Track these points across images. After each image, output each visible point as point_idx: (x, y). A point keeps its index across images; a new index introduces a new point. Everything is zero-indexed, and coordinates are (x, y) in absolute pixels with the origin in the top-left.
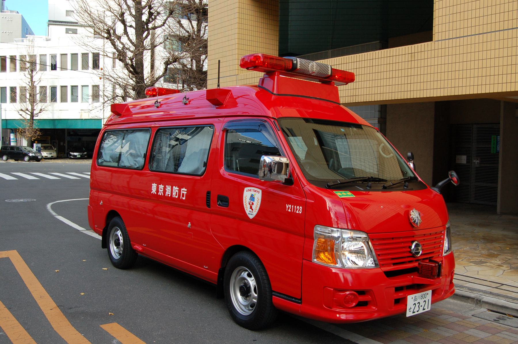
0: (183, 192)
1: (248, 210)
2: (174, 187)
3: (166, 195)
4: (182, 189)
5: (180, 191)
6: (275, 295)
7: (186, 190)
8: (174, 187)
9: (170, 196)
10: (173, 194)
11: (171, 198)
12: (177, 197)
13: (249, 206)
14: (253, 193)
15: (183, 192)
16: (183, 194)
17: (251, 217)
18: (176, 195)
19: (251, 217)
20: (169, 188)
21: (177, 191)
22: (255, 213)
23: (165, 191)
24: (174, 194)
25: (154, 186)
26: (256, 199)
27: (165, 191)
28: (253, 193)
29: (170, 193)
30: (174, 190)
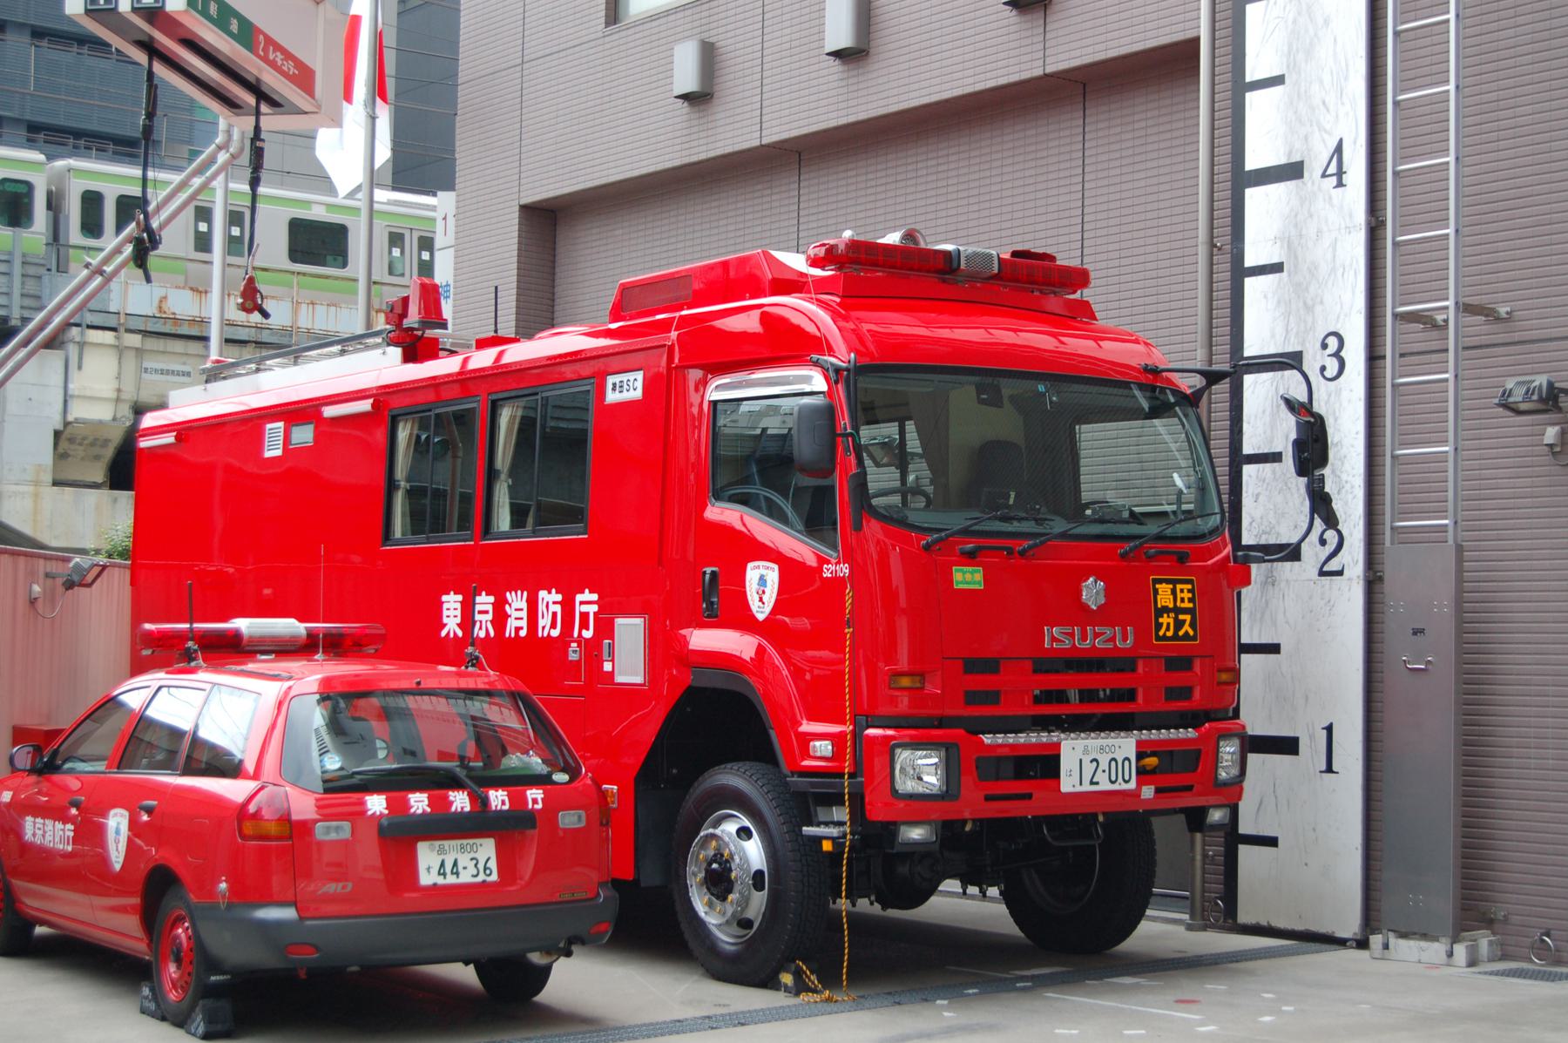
0: (585, 608)
1: (754, 605)
2: (543, 594)
3: (510, 631)
4: (579, 598)
5: (568, 605)
6: (687, 458)
7: (595, 597)
8: (543, 594)
9: (523, 633)
10: (541, 623)
11: (35, 816)
12: (555, 633)
13: (757, 597)
14: (764, 572)
15: (585, 608)
16: (584, 616)
17: (761, 617)
18: (553, 626)
19: (761, 617)
20: (517, 603)
21: (558, 608)
22: (768, 609)
23: (500, 618)
24: (544, 621)
25: (452, 604)
26: (769, 583)
27: (500, 618)
28: (764, 572)
29: (524, 623)
30: (541, 607)
